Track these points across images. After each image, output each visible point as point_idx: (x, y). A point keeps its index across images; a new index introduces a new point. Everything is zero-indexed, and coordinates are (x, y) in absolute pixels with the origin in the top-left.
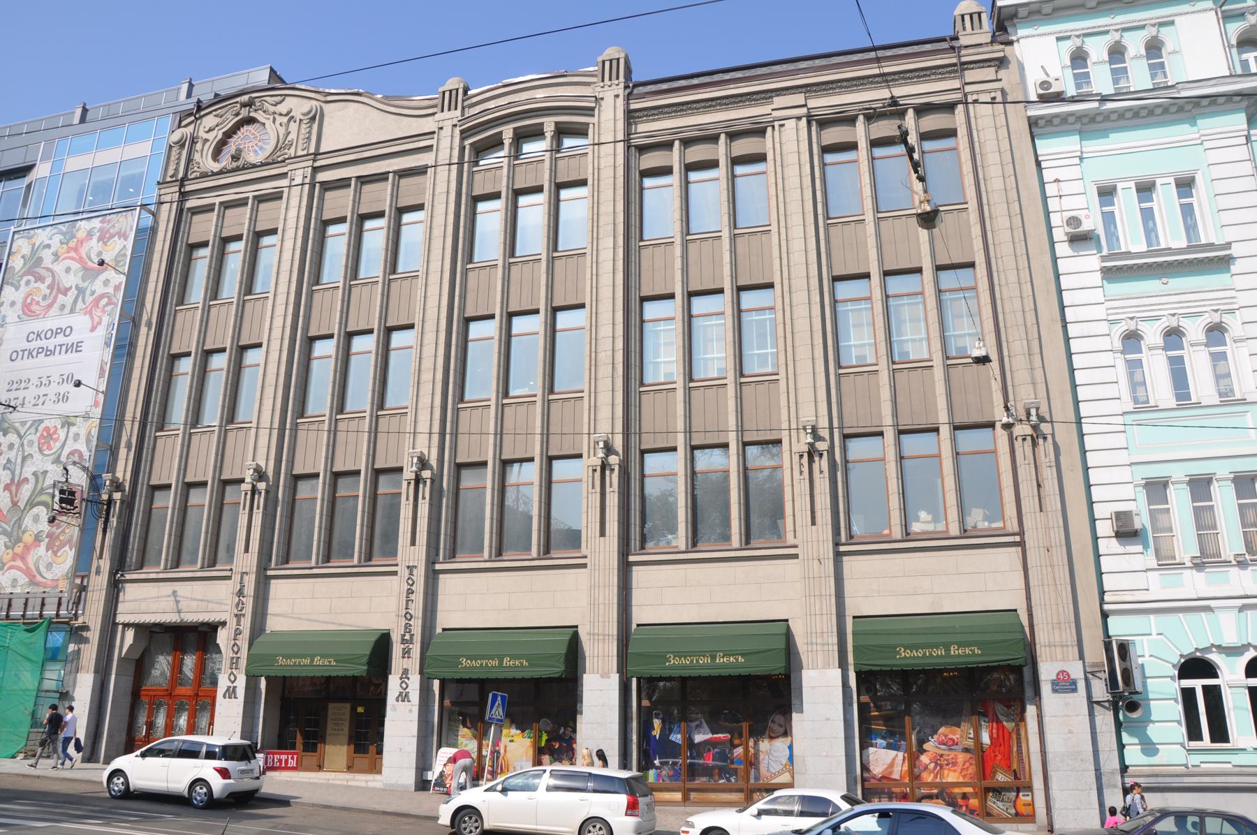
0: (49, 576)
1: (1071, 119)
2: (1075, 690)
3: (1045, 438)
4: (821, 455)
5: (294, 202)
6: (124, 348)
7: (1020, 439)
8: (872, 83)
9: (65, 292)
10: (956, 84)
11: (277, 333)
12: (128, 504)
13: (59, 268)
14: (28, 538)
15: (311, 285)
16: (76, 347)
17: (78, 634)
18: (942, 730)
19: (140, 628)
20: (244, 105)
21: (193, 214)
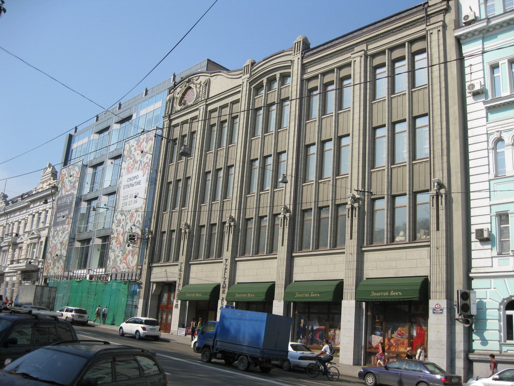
0: (132, 265)
3: (442, 196)
6: (152, 182)
8: (393, 33)
9: (137, 163)
12: (154, 239)
13: (136, 154)
14: (127, 252)
15: (206, 151)
16: (139, 183)
17: (139, 285)
18: (399, 329)
19: (158, 283)
20: (187, 82)
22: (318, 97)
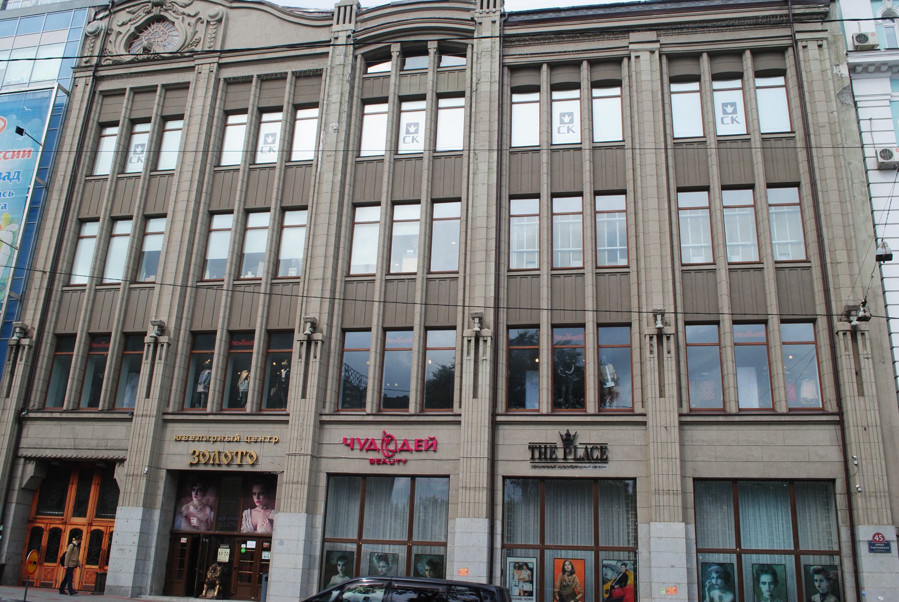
1: (884, 68)
2: (889, 551)
4: (668, 338)
5: (201, 92)
7: (841, 334)
10: (787, 32)
11: (182, 206)
19: (41, 462)
21: (104, 96)
22: (114, 140)
